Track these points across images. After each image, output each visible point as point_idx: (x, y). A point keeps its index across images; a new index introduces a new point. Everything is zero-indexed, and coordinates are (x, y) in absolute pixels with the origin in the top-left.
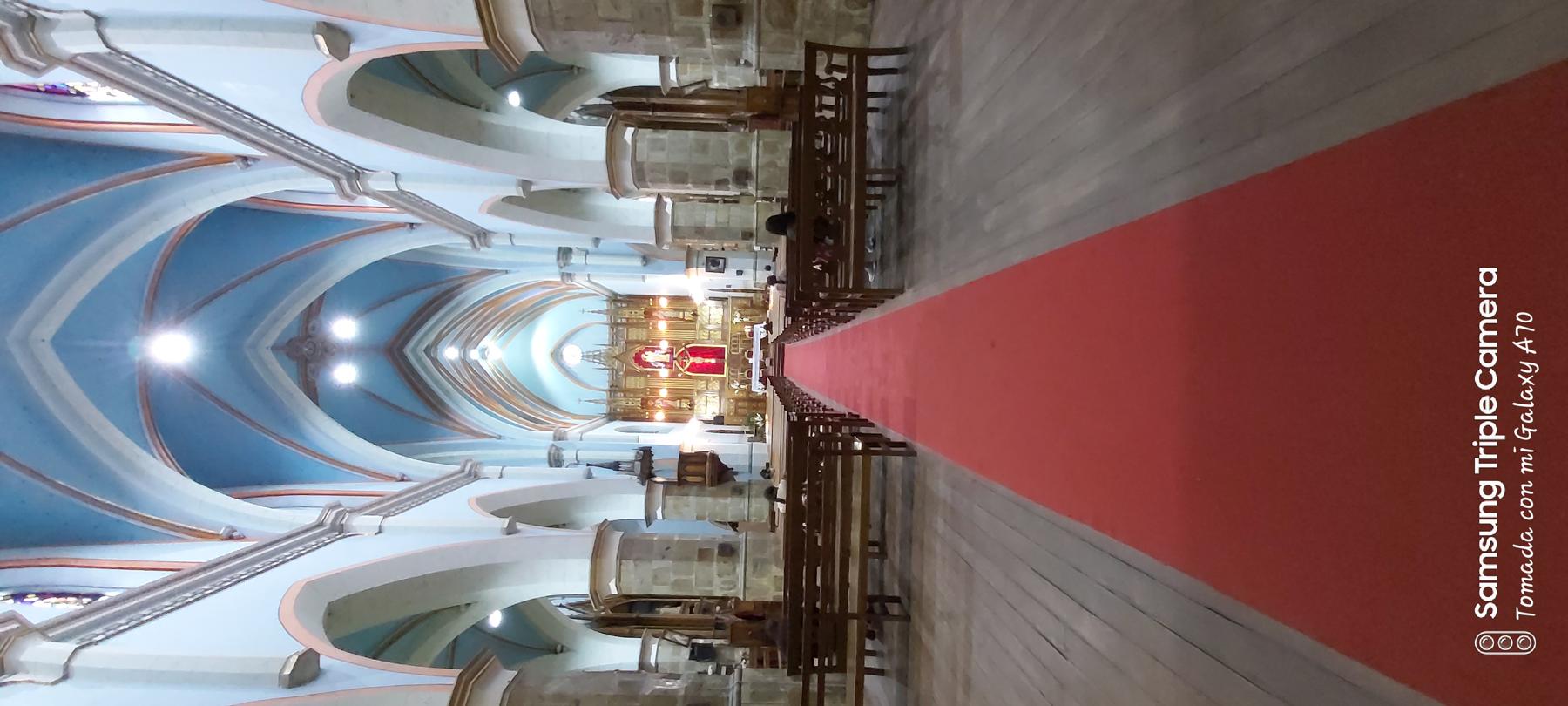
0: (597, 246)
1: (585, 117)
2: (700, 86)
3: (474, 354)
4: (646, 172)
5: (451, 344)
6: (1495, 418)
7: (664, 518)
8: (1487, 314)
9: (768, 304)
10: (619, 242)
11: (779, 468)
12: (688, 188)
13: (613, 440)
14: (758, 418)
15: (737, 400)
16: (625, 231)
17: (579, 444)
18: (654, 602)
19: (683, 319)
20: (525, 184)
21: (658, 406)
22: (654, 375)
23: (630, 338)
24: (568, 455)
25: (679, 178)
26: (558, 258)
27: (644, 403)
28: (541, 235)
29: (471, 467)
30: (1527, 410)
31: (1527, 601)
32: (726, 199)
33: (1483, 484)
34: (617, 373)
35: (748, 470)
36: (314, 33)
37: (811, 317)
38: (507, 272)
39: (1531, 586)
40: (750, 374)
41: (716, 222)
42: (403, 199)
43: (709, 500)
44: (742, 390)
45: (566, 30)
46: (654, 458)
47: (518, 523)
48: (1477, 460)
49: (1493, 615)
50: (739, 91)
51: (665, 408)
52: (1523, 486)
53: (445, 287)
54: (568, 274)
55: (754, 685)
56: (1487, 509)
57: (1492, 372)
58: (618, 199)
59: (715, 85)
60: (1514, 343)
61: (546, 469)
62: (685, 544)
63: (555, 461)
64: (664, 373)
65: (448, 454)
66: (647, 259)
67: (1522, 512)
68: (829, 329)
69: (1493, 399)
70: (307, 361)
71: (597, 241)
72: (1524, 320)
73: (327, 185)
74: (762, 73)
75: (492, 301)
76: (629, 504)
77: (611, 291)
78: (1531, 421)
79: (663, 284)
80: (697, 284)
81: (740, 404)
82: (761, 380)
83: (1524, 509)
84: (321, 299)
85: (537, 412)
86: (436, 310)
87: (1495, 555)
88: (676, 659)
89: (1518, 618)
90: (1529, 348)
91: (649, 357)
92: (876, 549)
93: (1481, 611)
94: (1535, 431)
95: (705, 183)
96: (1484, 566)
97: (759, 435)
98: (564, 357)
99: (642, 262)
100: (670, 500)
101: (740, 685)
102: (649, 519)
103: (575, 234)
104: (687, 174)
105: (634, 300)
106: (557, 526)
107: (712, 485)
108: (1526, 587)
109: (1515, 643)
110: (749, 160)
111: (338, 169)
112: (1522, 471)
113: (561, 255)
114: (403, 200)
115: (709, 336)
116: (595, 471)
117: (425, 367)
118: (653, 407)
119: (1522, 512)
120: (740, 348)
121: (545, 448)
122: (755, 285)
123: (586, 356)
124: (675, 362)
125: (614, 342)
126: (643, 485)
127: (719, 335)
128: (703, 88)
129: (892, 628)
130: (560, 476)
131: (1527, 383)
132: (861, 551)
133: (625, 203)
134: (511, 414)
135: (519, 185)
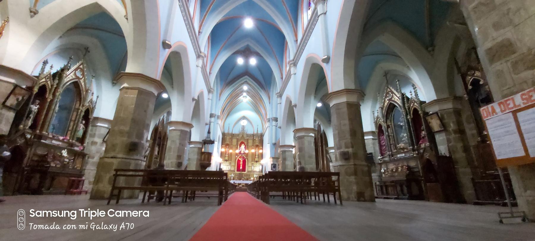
0: (278, 128)
3: (245, 94)
5: (248, 88)
6: (98, 216)
8: (133, 213)
10: (280, 135)
20: (295, 106)
22: (237, 148)
23: (249, 140)
24: (213, 119)
26: (274, 118)
28: (281, 112)
30: (101, 227)
31: (35, 227)
33: (75, 212)
38: (270, 103)
42: (289, 76)
43: (195, 163)
48: (84, 210)
49: (31, 215)
51: (226, 151)
52: (75, 226)
53: (265, 87)
56: (67, 213)
57: (114, 215)
59: (331, 164)
60: (124, 223)
64: (237, 151)
66: (275, 145)
67: (66, 225)
69: (104, 215)
71: (280, 128)
72: (131, 226)
75: (261, 99)
76: (196, 136)
77: (264, 135)
78: (97, 229)
79: (267, 151)
83: (67, 226)
85: (227, 111)
86: (259, 85)
87: (51, 216)
89: (30, 224)
90: (122, 228)
91: (243, 146)
93: (32, 211)
94: (94, 230)
96: (47, 212)
98: (243, 120)
99: (274, 143)
100: (196, 150)
103: (282, 121)
108: (40, 227)
109: (21, 223)
111: (296, 61)
112: (80, 225)
117: (240, 82)
119: (66, 225)
120: (245, 178)
124: (241, 155)
125: (247, 135)
127: (250, 170)
131: (110, 227)
133: (292, 134)
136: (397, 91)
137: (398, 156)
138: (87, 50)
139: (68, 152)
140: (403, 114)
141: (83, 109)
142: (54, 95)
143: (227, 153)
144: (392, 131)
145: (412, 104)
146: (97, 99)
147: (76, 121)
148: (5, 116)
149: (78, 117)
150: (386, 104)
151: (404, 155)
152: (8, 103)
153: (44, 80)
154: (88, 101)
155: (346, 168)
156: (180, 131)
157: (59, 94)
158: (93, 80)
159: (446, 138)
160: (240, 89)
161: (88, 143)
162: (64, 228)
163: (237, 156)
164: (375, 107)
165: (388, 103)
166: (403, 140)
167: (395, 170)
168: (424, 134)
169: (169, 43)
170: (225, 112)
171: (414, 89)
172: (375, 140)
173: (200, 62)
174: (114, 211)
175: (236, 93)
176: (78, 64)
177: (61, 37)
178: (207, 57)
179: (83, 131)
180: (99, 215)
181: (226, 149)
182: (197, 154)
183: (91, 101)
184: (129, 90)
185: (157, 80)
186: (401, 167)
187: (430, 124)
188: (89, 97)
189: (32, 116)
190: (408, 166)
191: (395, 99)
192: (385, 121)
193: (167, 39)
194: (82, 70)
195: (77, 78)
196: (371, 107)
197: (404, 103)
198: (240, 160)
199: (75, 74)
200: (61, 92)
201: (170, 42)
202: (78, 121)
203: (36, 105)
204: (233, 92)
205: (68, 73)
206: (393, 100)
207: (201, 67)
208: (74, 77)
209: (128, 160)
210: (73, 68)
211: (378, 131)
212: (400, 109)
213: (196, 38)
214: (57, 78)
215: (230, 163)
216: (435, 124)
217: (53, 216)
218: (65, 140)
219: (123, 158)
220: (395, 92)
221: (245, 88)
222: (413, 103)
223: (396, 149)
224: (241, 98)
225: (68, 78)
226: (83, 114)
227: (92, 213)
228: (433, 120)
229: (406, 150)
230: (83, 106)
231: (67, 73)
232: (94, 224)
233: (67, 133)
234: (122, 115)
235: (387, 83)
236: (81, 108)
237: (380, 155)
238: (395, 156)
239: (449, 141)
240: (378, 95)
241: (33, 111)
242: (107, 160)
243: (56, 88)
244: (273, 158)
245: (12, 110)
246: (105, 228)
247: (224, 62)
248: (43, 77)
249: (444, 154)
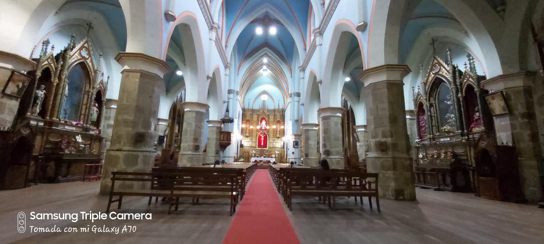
0: (301, 105)
1: (343, 101)
2: (357, 139)
3: (265, 67)
5: (268, 61)
6: (100, 219)
7: (209, 127)
8: (135, 216)
9: (282, 163)
11: (225, 166)
12: (322, 134)
14: (242, 160)
15: (248, 152)
18: (180, 124)
19: (277, 134)
20: (321, 82)
22: (258, 124)
23: (270, 116)
24: (231, 96)
25: (326, 131)
26: (296, 93)
28: (304, 87)
29: (229, 66)
30: (102, 230)
32: (319, 148)
33: (77, 215)
35: (224, 156)
36: (364, 21)
37: (280, 177)
38: (291, 77)
39: (41, 231)
40: (258, 157)
42: (314, 47)
43: (214, 142)
44: (252, 154)
45: (372, 94)
46: (229, 123)
48: (85, 212)
49: (31, 218)
50: (356, 152)
52: (76, 228)
53: (287, 59)
54: (292, 96)
55: (150, 157)
56: (68, 216)
57: (116, 218)
59: (358, 144)
60: (126, 225)
61: (227, 89)
62: (200, 134)
64: (258, 127)
65: (233, 59)
66: (297, 122)
67: (67, 228)
68: (275, 184)
69: (106, 218)
70: (263, 21)
71: (303, 105)
73: (317, 25)
74: (364, 160)
75: (282, 72)
76: (214, 115)
79: (289, 127)
80: (289, 138)
81: (247, 153)
82: (256, 161)
83: (68, 229)
84: (283, 25)
85: (246, 86)
87: (52, 219)
88: (160, 131)
89: (30, 227)
91: (264, 122)
92: (195, 201)
93: (33, 214)
94: (95, 233)
96: (48, 215)
97: (236, 160)
100: (215, 129)
101: (150, 152)
102: (209, 122)
105: (283, 117)
106: (208, 92)
107: (220, 143)
108: (41, 229)
110: (333, 155)
111: (322, 29)
112: (81, 228)
114: (313, 47)
116: (226, 104)
119: (67, 228)
120: (267, 154)
122: (289, 159)
124: (262, 131)
125: (268, 111)
126: (221, 120)
127: (271, 146)
128: (356, 140)
129: (166, 208)
132: (195, 195)
133: (316, 113)
136: (446, 62)
137: (442, 140)
138: (90, 26)
139: (82, 137)
140: (453, 92)
141: (93, 91)
142: (60, 78)
143: (248, 130)
144: (435, 111)
145: (466, 79)
146: (108, 79)
147: (88, 105)
148: (7, 105)
149: (89, 100)
150: (430, 78)
151: (449, 139)
152: (8, 91)
153: (46, 62)
154: (98, 82)
155: (382, 161)
156: (195, 113)
157: (65, 77)
158: (101, 59)
159: (510, 124)
160: (260, 62)
161: (104, 125)
162: (65, 231)
163: (258, 133)
164: (416, 82)
165: (433, 78)
166: (448, 121)
167: (436, 156)
168: (478, 116)
169: (173, 14)
170: (244, 87)
171: (469, 60)
172: (413, 120)
173: (214, 35)
174: (115, 213)
175: (255, 67)
176: (82, 43)
177: (56, 13)
178: (221, 28)
179: (97, 114)
180: (101, 218)
181: (246, 125)
182: (215, 134)
183: (102, 82)
184: (131, 73)
185: (161, 60)
186: (444, 154)
187: (490, 105)
188: (99, 78)
189: (39, 102)
190: (453, 152)
191: (443, 72)
192: (428, 98)
193: (170, 10)
194: (87, 49)
195: (83, 58)
196: (411, 82)
197: (454, 78)
198: (261, 136)
199: (80, 54)
200: (67, 75)
201: (174, 13)
202: (90, 105)
203: (43, 90)
204: (252, 66)
205: (72, 53)
206: (441, 74)
207: (215, 41)
208: (79, 57)
209: (135, 153)
210: (78, 47)
211: (417, 110)
212: (449, 86)
213: (208, 8)
214: (61, 60)
215: (251, 139)
216: (497, 105)
217: (54, 218)
218: (79, 125)
219: (128, 151)
220: (444, 64)
221: (265, 60)
222: (467, 78)
223: (439, 133)
224: (261, 71)
225: (73, 58)
226: (94, 96)
227: (94, 216)
228: (495, 100)
229: (451, 134)
230: (93, 88)
231: (71, 53)
232: (96, 226)
233: (80, 117)
234: (125, 102)
235: (434, 52)
236: (91, 90)
237: (418, 138)
238: (437, 140)
239: (513, 127)
240: (421, 67)
241: (38, 97)
242: (112, 153)
243: (61, 71)
244: (295, 135)
245: (14, 98)
246: (107, 231)
247: (241, 33)
248: (45, 60)
249: (507, 143)
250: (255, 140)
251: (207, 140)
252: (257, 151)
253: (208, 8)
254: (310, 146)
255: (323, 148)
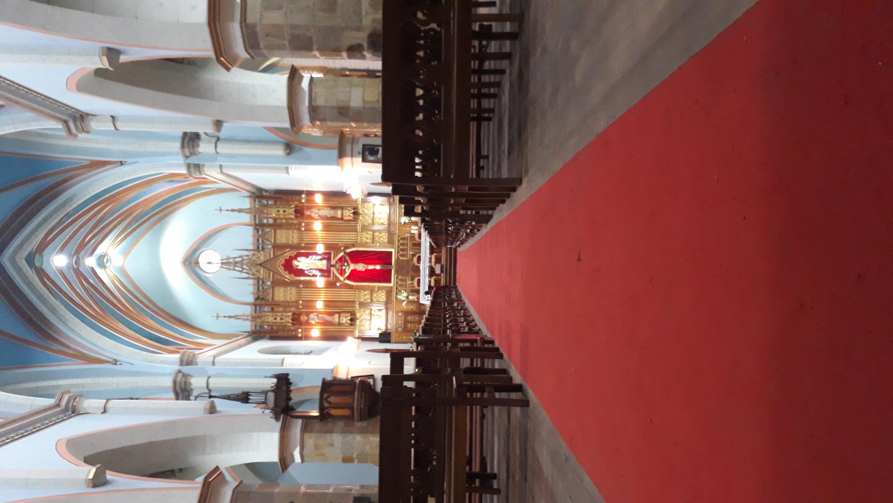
3: (90, 262)
4: (260, 35)
10: (256, 126)
12: (315, 57)
13: (251, 364)
15: (406, 313)
16: (252, 112)
17: (211, 370)
20: (112, 53)
21: (313, 322)
22: (309, 285)
23: (278, 242)
24: (197, 383)
26: (183, 147)
27: (296, 319)
34: (263, 282)
38: (121, 163)
41: (364, 101)
43: (358, 438)
44: (412, 302)
47: (108, 472)
58: (228, 69)
63: (182, 391)
64: (320, 282)
71: (218, 124)
81: (409, 318)
91: (302, 263)
95: (335, 50)
100: (310, 440)
102: (285, 461)
104: (310, 39)
105: (283, 196)
107: (361, 419)
113: (186, 142)
115: (373, 238)
116: (220, 404)
118: (308, 323)
121: (170, 374)
123: (227, 263)
126: (277, 419)
127: (384, 237)
130: (195, 407)
134: (132, 333)
135: (103, 55)
213: (9, 423)
215: (363, 305)
244: (341, 154)
250: (366, 292)
251: (350, 465)
252: (400, 285)
253: (9, 423)
254: (367, 106)
255: (363, 57)
